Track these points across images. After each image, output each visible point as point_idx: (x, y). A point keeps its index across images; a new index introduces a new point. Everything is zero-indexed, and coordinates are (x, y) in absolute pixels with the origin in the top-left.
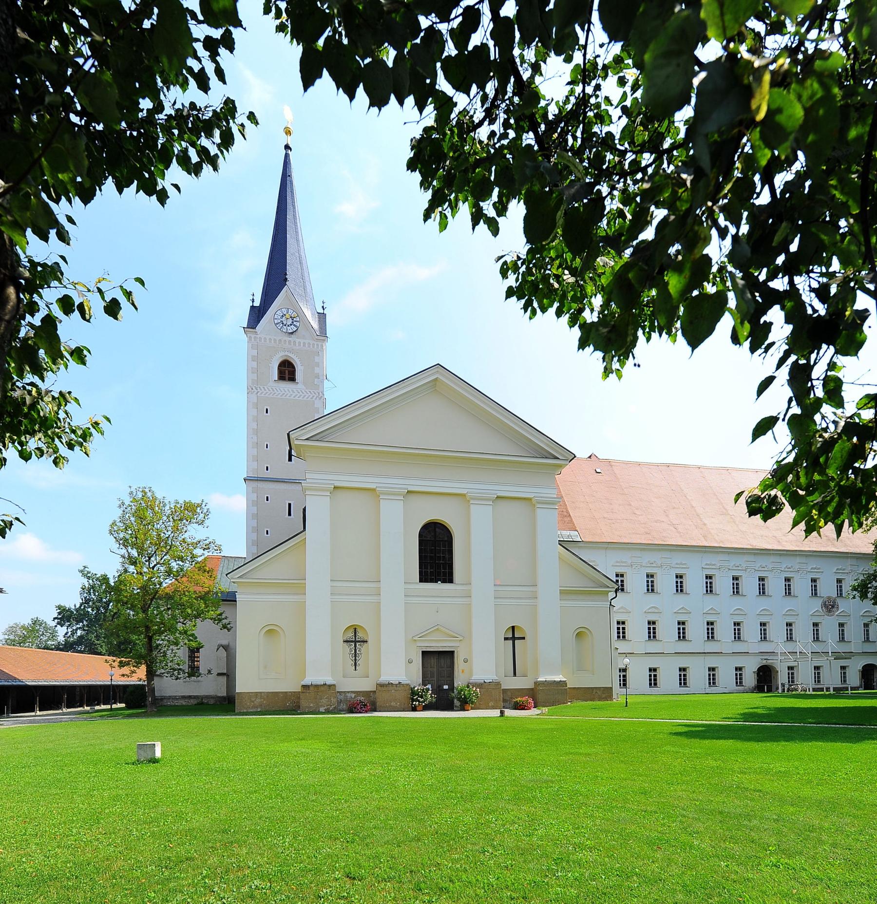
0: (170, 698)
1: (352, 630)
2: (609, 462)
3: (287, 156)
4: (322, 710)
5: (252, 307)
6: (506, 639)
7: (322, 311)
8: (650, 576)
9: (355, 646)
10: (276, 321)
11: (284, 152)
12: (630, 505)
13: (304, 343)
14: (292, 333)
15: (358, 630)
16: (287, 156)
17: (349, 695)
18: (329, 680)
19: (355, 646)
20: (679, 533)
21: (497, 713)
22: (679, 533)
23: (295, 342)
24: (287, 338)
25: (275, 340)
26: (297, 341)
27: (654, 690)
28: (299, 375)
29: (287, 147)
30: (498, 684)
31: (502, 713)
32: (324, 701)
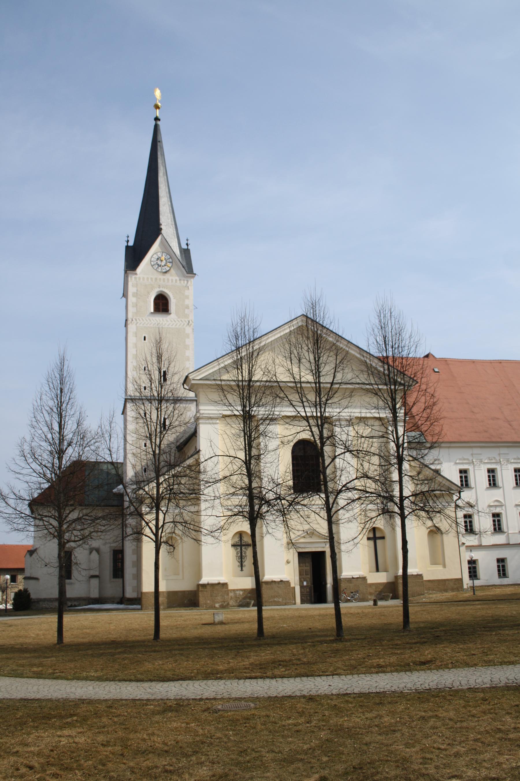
0: (45, 600)
1: (238, 536)
2: (445, 361)
3: (156, 129)
4: (217, 605)
5: (127, 247)
6: (369, 539)
7: (186, 247)
8: (491, 471)
9: (241, 549)
10: (152, 263)
11: (154, 122)
12: (468, 403)
13: (148, 278)
14: (166, 272)
15: (244, 535)
16: (156, 129)
17: (238, 592)
18: (222, 580)
19: (241, 549)
20: (514, 429)
21: (371, 603)
22: (514, 429)
23: (168, 280)
24: (161, 277)
25: (151, 279)
26: (170, 278)
27: (505, 581)
28: (172, 306)
29: (157, 119)
30: (364, 579)
31: (375, 604)
32: (219, 598)
